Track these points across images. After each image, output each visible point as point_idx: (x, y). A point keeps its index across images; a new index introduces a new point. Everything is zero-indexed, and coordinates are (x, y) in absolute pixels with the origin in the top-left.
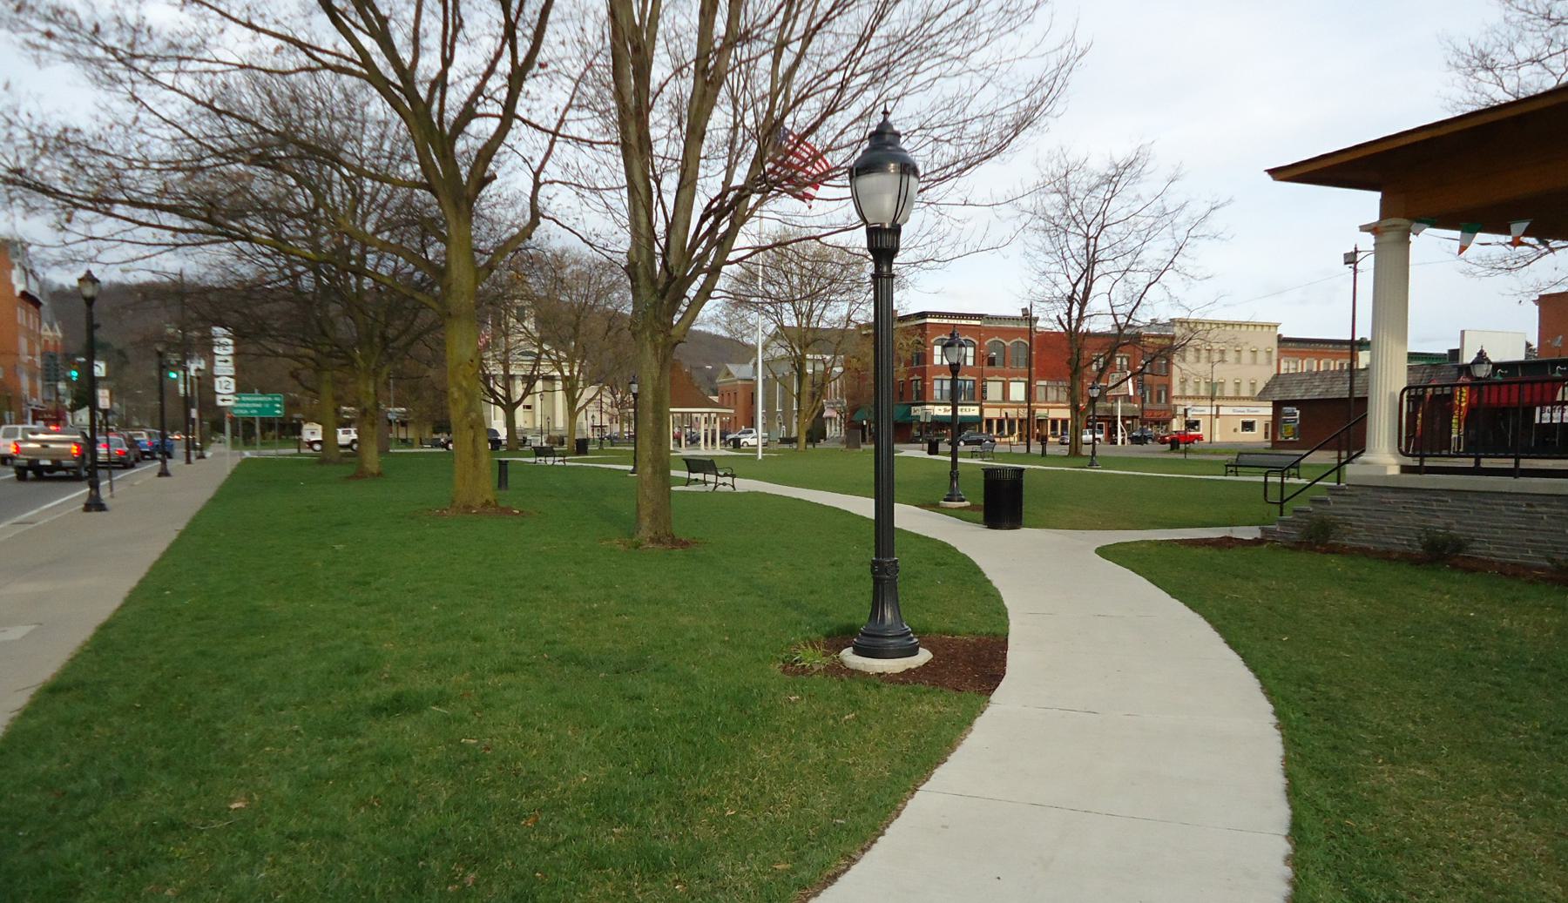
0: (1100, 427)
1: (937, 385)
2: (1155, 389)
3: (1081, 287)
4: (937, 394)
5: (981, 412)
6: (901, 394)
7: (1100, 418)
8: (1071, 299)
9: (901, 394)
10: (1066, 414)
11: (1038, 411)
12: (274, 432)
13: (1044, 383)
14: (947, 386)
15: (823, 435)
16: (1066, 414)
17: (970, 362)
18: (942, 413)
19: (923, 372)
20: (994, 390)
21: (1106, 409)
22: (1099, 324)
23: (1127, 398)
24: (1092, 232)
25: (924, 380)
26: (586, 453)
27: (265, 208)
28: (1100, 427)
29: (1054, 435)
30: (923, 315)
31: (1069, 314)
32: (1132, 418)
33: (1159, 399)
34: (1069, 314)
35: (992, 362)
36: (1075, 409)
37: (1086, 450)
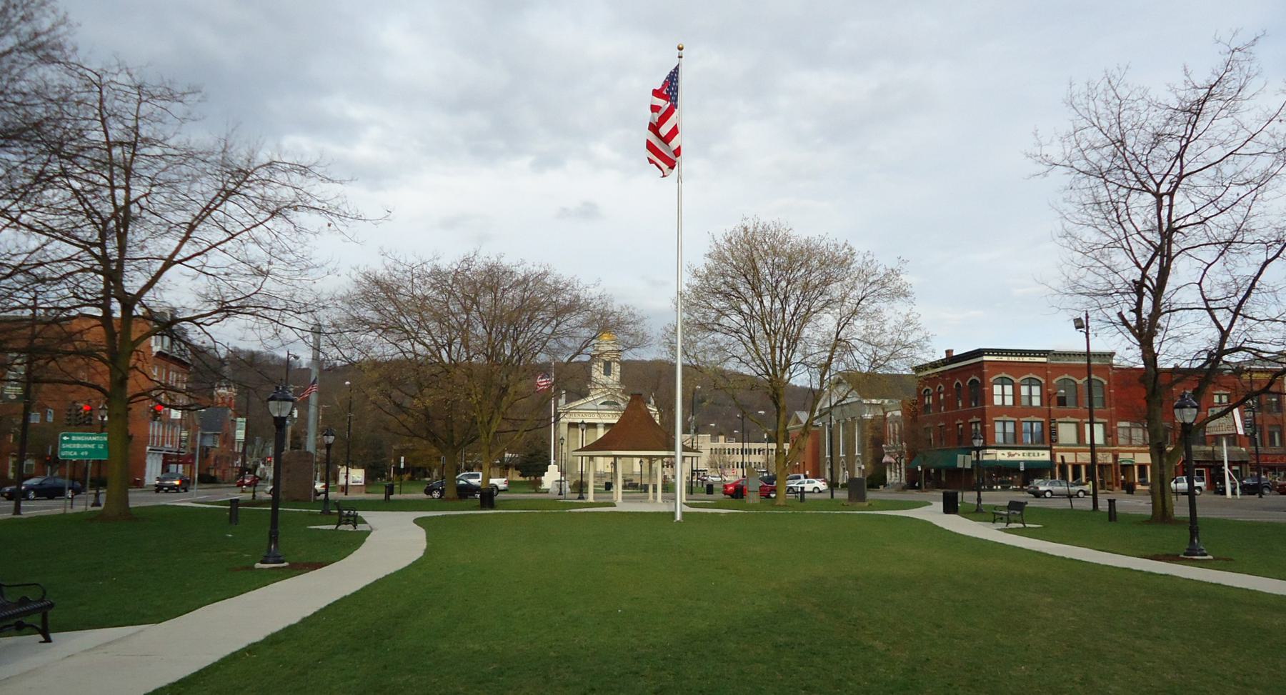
0: (1200, 474)
1: (999, 427)
2: (1266, 429)
3: (1154, 271)
4: (999, 438)
5: (1053, 456)
6: (960, 438)
7: (1199, 464)
8: (1138, 287)
9: (960, 438)
10: (1145, 458)
11: (1121, 456)
12: (406, 477)
13: (1127, 424)
14: (1010, 428)
15: (883, 481)
16: (1145, 458)
17: (1036, 402)
18: (1041, 458)
19: (982, 414)
20: (1067, 433)
21: (1205, 454)
22: (1184, 342)
23: (1233, 439)
24: (1164, 188)
25: (983, 423)
26: (492, 506)
27: (89, 216)
28: (1200, 474)
29: (1143, 483)
30: (980, 352)
31: (1138, 310)
32: (1240, 463)
33: (1272, 442)
34: (1138, 310)
35: (1062, 401)
36: (1157, 449)
37: (1180, 509)
